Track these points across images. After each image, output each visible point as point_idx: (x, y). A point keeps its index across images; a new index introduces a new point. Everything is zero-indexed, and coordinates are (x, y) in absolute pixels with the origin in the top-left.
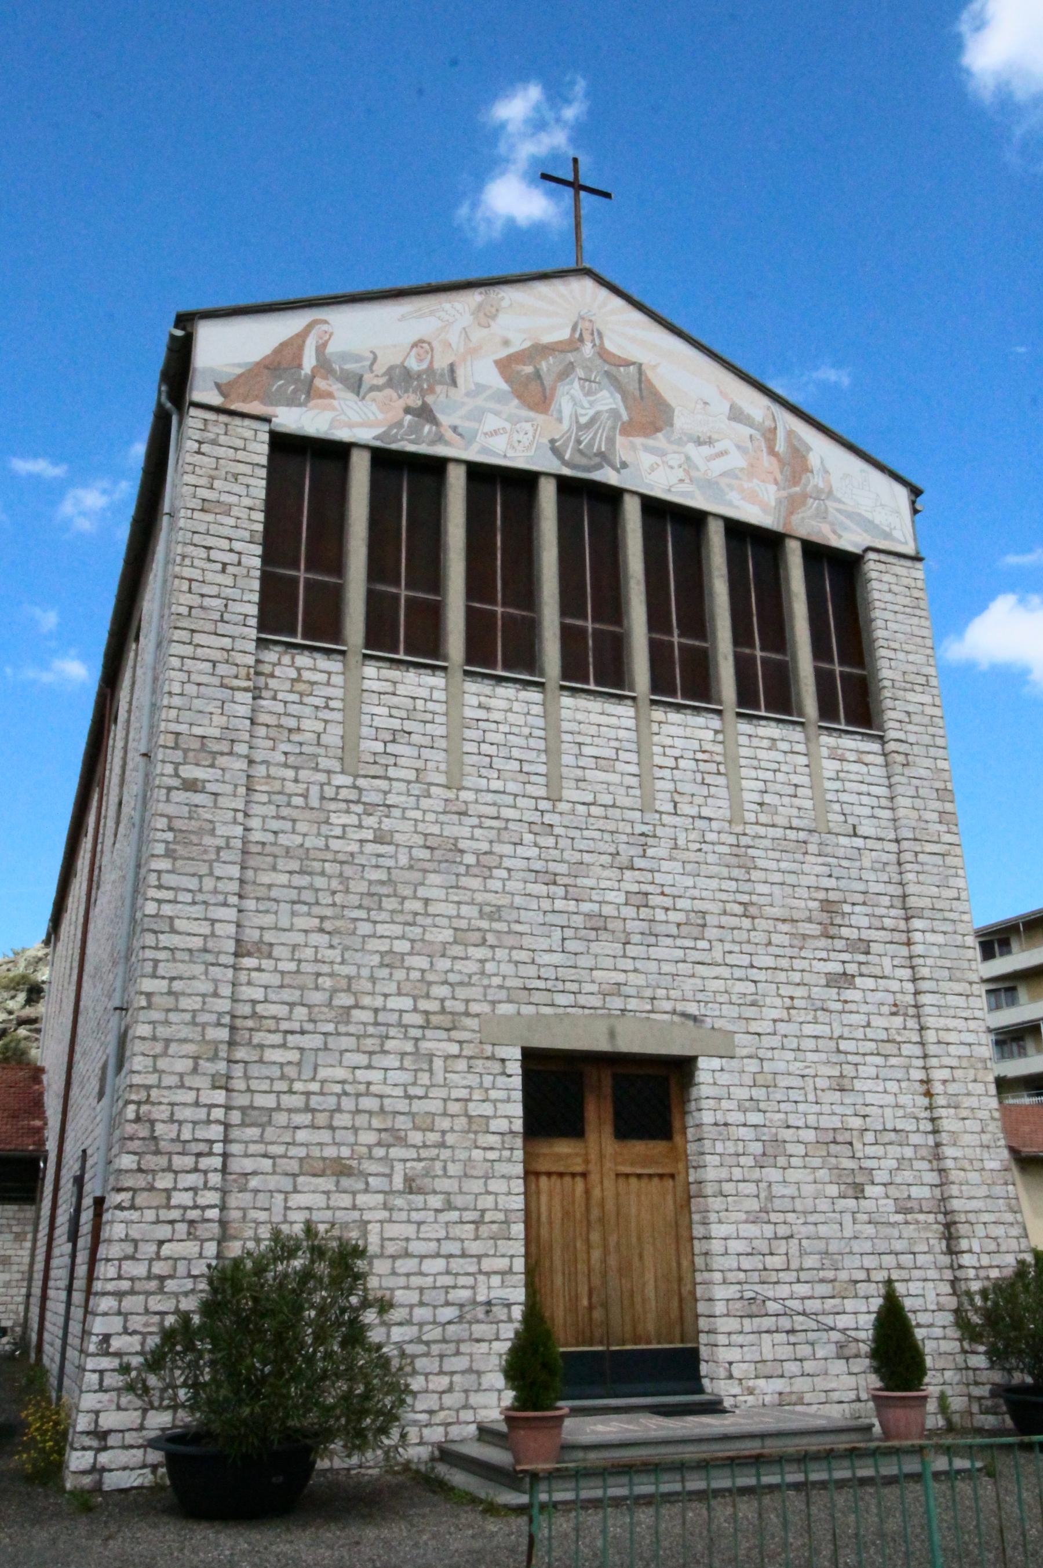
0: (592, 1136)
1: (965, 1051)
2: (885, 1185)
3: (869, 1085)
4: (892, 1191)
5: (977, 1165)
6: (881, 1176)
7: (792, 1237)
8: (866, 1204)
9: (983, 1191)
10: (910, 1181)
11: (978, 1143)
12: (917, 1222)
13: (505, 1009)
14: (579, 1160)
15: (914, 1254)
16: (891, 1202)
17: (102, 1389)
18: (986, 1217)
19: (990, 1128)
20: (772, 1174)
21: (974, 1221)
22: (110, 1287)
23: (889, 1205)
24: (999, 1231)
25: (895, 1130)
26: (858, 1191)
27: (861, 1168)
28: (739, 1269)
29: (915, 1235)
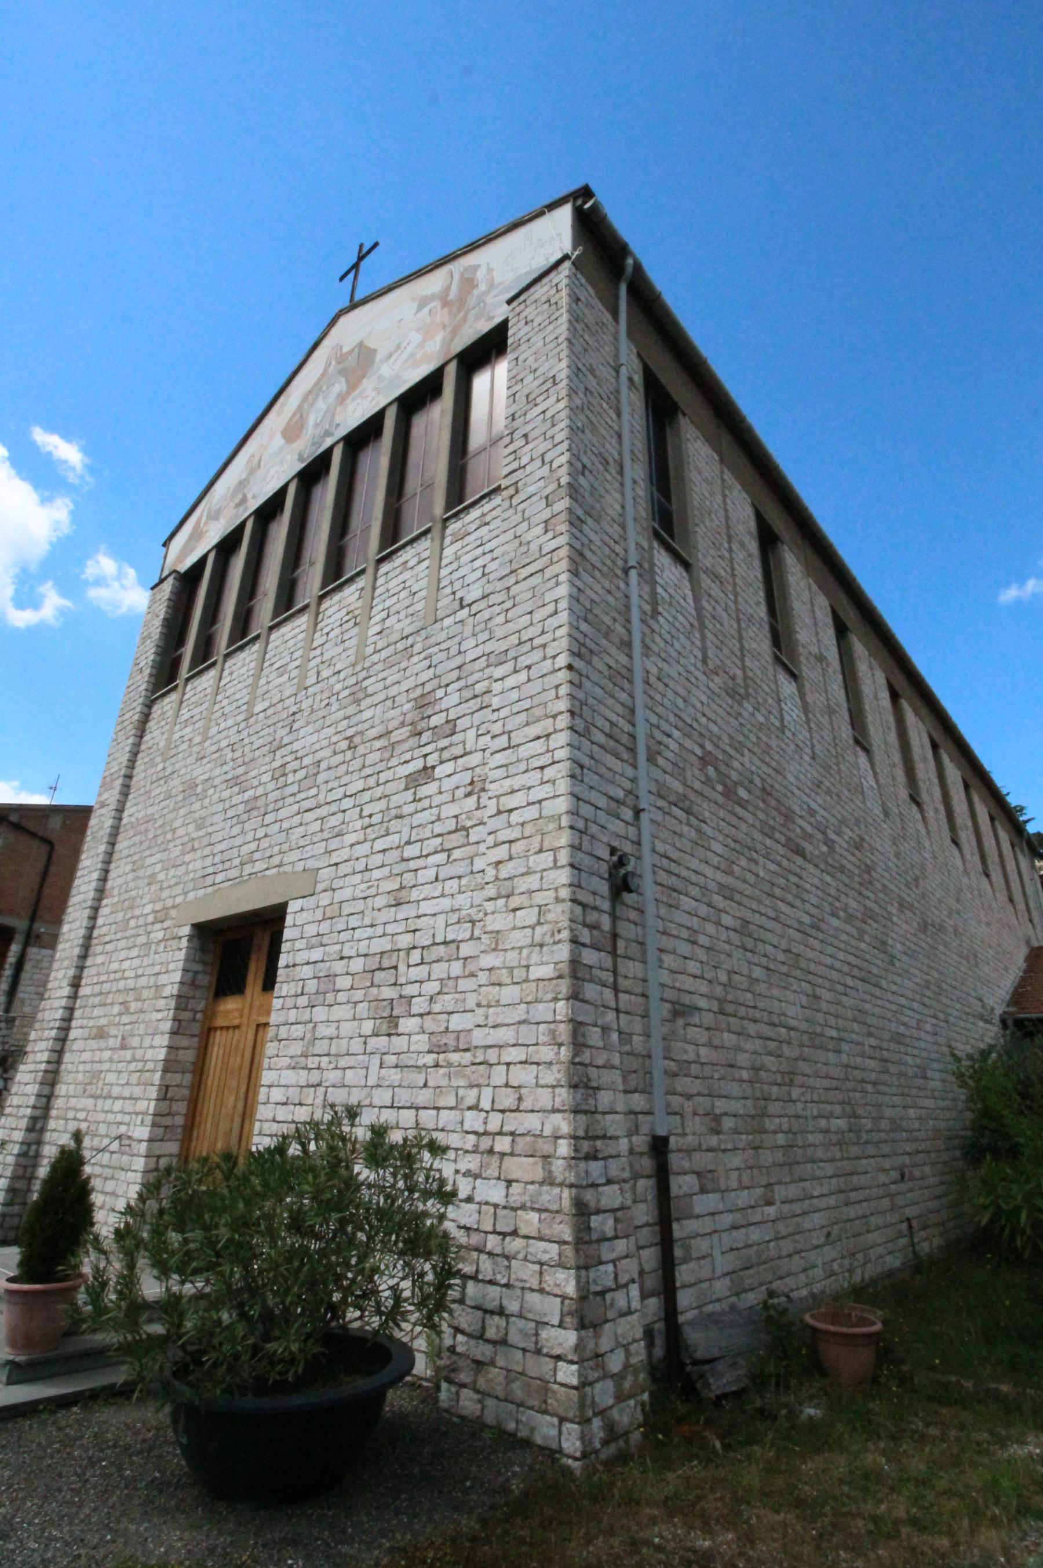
0: (249, 990)
1: (532, 812)
2: (421, 1015)
3: (427, 891)
4: (429, 1024)
5: (519, 974)
6: (419, 1005)
7: (319, 1085)
8: (399, 1043)
9: (519, 1013)
10: (450, 1009)
11: (529, 941)
12: (450, 1065)
13: (191, 896)
14: (237, 1014)
15: (438, 1109)
16: (425, 1037)
17: (925, 1227)
18: (514, 1054)
19: (550, 917)
20: (320, 1013)
21: (493, 1060)
22: (14, 1111)
23: (421, 1042)
24: (523, 1076)
25: (445, 943)
26: (391, 1025)
27: (401, 997)
28: (274, 1120)
29: (444, 1082)
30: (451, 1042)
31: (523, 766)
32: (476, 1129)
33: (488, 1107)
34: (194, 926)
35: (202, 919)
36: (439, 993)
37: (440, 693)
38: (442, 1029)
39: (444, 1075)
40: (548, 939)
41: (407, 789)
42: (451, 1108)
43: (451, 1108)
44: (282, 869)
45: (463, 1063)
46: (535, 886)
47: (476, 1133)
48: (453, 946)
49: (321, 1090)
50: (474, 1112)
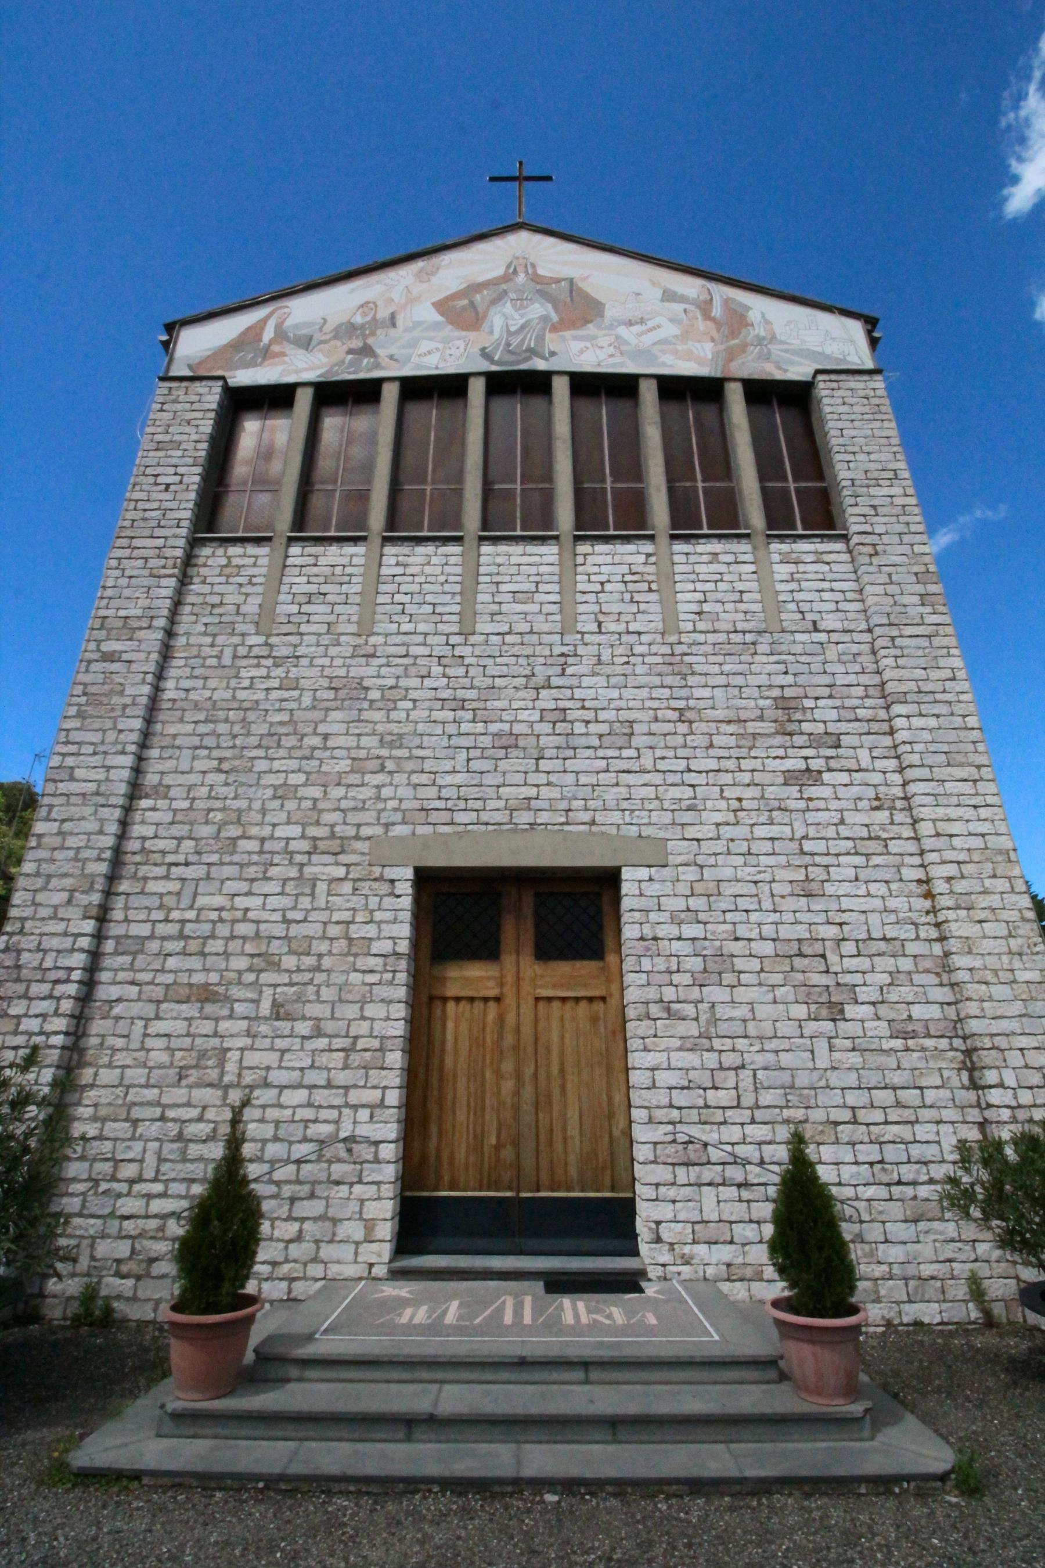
10: (910, 999)
30: (919, 1028)
31: (954, 800)
32: (1007, 1103)
33: (1014, 1085)
34: (418, 870)
35: (430, 863)
36: (150, 1019)
37: (809, 703)
38: (905, 1016)
39: (920, 1058)
40: (1026, 950)
41: (168, 787)
42: (937, 1087)
43: (937, 1087)
44: (594, 828)
45: (941, 1047)
46: (160, 926)
47: (1008, 1107)
48: (898, 943)
49: (746, 1075)
50: (1001, 1090)
